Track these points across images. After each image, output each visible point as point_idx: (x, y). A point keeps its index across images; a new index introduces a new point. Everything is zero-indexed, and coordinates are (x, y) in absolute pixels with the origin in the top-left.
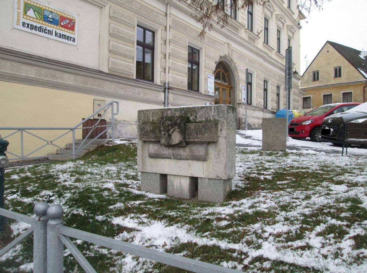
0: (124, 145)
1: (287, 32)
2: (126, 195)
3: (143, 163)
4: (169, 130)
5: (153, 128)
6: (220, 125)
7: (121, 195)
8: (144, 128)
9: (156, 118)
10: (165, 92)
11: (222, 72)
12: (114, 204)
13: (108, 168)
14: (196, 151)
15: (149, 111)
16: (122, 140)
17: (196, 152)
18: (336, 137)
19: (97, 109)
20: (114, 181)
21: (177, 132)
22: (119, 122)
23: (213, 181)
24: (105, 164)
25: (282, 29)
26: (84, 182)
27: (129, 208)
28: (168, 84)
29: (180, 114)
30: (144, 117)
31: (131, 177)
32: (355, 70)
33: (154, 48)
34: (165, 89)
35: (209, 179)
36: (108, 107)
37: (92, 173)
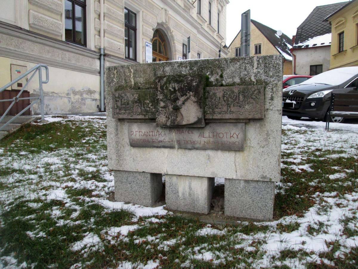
0: (60, 123)
1: (217, 4)
2: (94, 212)
3: (119, 156)
4: (177, 99)
5: (139, 96)
6: (271, 90)
7: (85, 215)
8: (120, 97)
9: (141, 80)
10: (100, 59)
11: (159, 41)
12: (80, 238)
13: (46, 160)
14: (225, 135)
15: (129, 68)
16: (55, 117)
17: (225, 137)
18: (299, 109)
19: (16, 76)
20: (64, 185)
21: (192, 102)
22: (47, 94)
23: (254, 184)
24: (39, 152)
25: (212, 2)
26: (10, 189)
27: (113, 246)
28: (104, 50)
29: (191, 72)
30: (119, 77)
31: (90, 176)
32: (274, 47)
33: (86, 6)
34: (100, 55)
35: (247, 181)
36: (33, 72)
37: (21, 172)
